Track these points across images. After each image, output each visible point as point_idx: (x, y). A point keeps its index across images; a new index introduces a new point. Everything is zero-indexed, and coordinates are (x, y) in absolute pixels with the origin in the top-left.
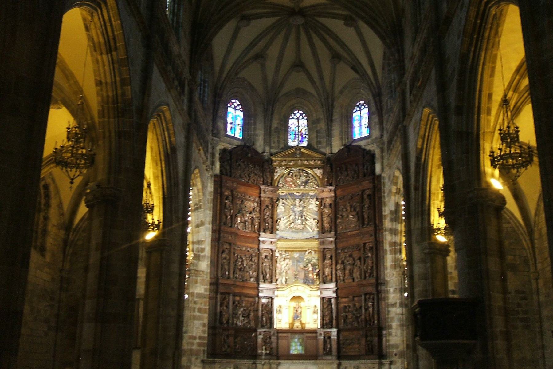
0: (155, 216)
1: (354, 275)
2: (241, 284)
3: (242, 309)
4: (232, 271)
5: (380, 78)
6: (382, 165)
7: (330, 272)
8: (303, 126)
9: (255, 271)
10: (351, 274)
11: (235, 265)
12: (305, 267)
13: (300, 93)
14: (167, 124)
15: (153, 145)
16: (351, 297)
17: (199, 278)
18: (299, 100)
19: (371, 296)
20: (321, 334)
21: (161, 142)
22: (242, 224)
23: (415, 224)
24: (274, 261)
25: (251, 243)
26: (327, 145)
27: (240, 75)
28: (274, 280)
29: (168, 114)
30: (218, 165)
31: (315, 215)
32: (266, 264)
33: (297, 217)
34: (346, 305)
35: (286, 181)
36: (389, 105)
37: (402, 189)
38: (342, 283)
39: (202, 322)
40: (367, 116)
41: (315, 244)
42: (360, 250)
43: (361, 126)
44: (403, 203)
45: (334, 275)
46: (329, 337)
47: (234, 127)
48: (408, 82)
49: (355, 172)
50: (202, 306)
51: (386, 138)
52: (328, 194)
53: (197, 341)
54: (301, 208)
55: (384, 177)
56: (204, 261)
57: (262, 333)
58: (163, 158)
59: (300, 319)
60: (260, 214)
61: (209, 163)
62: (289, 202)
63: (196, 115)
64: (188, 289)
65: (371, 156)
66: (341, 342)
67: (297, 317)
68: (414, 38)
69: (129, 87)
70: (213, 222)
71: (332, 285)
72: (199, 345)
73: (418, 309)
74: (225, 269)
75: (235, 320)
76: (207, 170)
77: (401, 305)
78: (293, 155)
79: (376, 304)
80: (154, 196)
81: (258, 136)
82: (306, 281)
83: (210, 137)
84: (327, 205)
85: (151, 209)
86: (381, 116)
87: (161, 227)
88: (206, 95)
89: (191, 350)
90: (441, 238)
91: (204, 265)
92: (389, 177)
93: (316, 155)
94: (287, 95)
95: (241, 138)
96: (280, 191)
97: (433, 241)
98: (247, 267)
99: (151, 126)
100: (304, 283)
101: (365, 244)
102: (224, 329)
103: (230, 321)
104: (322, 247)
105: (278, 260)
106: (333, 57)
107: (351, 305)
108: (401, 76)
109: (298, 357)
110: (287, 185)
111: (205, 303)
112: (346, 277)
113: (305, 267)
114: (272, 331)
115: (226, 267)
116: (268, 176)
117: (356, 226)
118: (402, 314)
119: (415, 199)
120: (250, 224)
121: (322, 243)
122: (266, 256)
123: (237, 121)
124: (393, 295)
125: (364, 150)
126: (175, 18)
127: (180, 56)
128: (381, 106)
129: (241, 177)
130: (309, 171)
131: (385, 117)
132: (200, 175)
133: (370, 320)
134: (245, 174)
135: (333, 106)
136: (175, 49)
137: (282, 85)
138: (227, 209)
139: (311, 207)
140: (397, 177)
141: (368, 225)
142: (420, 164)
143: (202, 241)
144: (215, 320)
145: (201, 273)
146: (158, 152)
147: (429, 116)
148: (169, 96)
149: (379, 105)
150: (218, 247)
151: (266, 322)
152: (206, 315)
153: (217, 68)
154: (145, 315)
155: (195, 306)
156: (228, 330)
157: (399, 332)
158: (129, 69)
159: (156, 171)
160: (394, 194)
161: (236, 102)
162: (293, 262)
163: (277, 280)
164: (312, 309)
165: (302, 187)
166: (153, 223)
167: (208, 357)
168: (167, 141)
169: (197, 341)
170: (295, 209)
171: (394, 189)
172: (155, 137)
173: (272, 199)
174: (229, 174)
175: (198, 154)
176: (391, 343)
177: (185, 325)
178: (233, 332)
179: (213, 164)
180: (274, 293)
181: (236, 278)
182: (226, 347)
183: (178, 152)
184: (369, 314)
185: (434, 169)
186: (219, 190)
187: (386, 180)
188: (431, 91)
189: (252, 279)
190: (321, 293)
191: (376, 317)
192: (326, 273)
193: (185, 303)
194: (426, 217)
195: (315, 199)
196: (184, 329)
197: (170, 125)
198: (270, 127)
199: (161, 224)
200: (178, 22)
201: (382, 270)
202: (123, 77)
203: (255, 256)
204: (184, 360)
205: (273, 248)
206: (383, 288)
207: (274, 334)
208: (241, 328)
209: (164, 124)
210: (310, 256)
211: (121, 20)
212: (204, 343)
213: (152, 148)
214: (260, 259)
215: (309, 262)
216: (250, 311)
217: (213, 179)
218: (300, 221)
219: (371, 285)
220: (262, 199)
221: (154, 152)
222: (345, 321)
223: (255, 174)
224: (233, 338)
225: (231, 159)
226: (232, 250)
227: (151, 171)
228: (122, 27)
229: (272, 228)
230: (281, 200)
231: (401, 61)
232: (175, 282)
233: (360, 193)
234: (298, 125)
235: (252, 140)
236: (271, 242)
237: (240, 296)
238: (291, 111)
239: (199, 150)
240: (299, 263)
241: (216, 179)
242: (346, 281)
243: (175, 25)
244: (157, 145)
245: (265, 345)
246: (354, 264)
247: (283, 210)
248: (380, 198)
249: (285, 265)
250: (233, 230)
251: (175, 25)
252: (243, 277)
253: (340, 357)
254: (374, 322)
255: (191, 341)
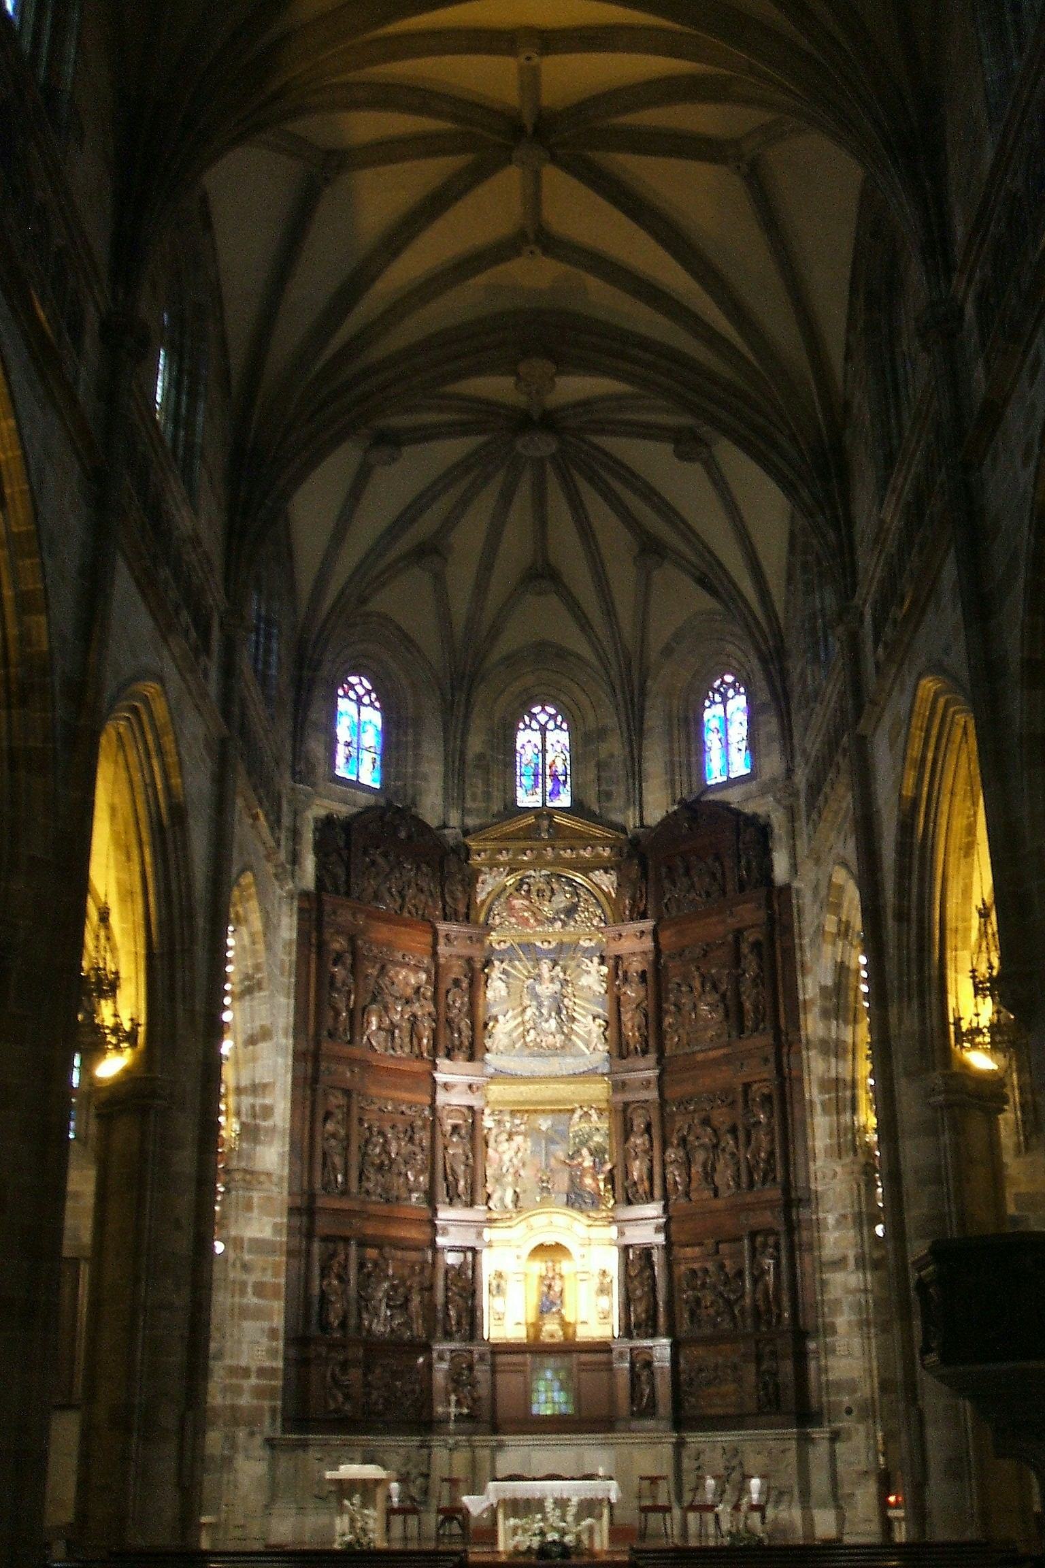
0: (126, 1007)
1: (717, 1178)
2: (384, 1209)
3: (386, 1285)
4: (354, 1174)
5: (779, 607)
6: (793, 854)
7: (645, 1171)
8: (558, 748)
9: (421, 1172)
10: (709, 1175)
11: (365, 1154)
12: (572, 1158)
13: (548, 654)
14: (157, 737)
15: (117, 801)
16: (710, 1242)
17: (256, 1196)
18: (544, 674)
19: (771, 1240)
20: (621, 1354)
21: (139, 790)
22: (383, 1034)
23: (900, 1020)
24: (479, 1141)
25: (408, 1089)
26: (628, 802)
27: (372, 606)
28: (480, 1198)
29: (160, 709)
30: (309, 863)
31: (597, 1004)
32: (456, 1149)
33: (545, 1011)
34: (696, 1266)
35: (512, 908)
36: (809, 681)
37: (857, 923)
38: (683, 1201)
39: (266, 1325)
40: (743, 718)
41: (599, 1090)
42: (734, 1102)
43: (726, 745)
44: (863, 960)
45: (657, 1181)
46: (648, 1364)
47: (354, 754)
48: (868, 611)
49: (713, 875)
50: (268, 1278)
51: (801, 778)
52: (635, 942)
53: (253, 1381)
54: (557, 987)
55: (798, 891)
56: (271, 1143)
57: (447, 1356)
58: (146, 836)
59: (559, 1312)
60: (436, 1005)
61: (283, 856)
62: (521, 968)
63: (243, 714)
64: (223, 1227)
65: (762, 832)
66: (683, 1377)
67: (549, 1304)
68: (883, 483)
69: (43, 619)
70: (299, 1029)
71: (653, 1210)
72: (259, 1393)
73: (931, 1268)
74: (334, 1168)
75: (365, 1316)
76: (276, 876)
77: (861, 1263)
78: (530, 833)
79: (784, 1261)
80: (117, 944)
81: (425, 778)
82: (576, 1199)
83: (285, 782)
84: (633, 975)
85: (109, 986)
86: (785, 717)
87: (141, 1039)
88: (273, 659)
89: (233, 1408)
90: (981, 1060)
91: (272, 1156)
92: (816, 889)
93: (598, 832)
94: (511, 660)
95: (378, 786)
96: (494, 936)
97: (956, 1068)
98: (400, 1159)
99: (107, 741)
100: (570, 1203)
101: (747, 1086)
102: (332, 1346)
103: (352, 1321)
104: (620, 1098)
105: (492, 1143)
106: (643, 551)
107: (710, 1266)
108: (848, 591)
109: (556, 1425)
110: (513, 920)
111: (276, 1267)
112: (694, 1185)
113: (572, 1158)
114: (477, 1349)
115: (338, 1160)
116: (459, 895)
117: (719, 1036)
118: (866, 1291)
119: (899, 948)
120: (406, 1034)
121: (619, 1087)
122: (455, 1128)
123: (363, 736)
124: (837, 1234)
125: (738, 813)
126: (182, 433)
127: (196, 541)
128: (784, 689)
129: (377, 897)
130: (579, 878)
131: (797, 721)
132: (258, 893)
133: (769, 1311)
134: (389, 889)
135: (643, 693)
136: (183, 520)
137: (495, 632)
138: (338, 991)
139: (585, 981)
140: (841, 888)
141: (756, 1029)
142: (912, 844)
143: (265, 1086)
144: (307, 1322)
145: (263, 1178)
146: (131, 820)
147: (935, 701)
148: (165, 653)
149: (778, 684)
150: (313, 1103)
151: (459, 1323)
152: (278, 1305)
153: (305, 580)
154: (96, 1304)
155: (245, 1277)
156: (344, 1347)
157: (856, 1342)
158: (43, 564)
159: (125, 876)
160: (829, 938)
161: (360, 684)
162: (536, 1143)
163: (489, 1197)
164: (595, 1283)
165: (558, 924)
166: (116, 1029)
167: (284, 1431)
168: (159, 786)
169: (253, 1381)
170: (539, 989)
171: (831, 926)
172: (123, 775)
173: (469, 960)
174: (342, 889)
175: (252, 831)
176: (832, 1377)
177: (215, 1334)
178: (361, 1353)
179: (295, 859)
180: (479, 1235)
181: (368, 1192)
182: (340, 1398)
183: (191, 822)
184: (766, 1286)
185: (952, 859)
186: (314, 935)
187: (807, 899)
188: (945, 622)
189: (415, 1195)
190: (621, 1233)
191: (785, 1299)
192: (636, 1175)
193: (217, 1268)
194: (934, 998)
195: (596, 960)
196: (213, 1346)
197: (168, 743)
198: (462, 754)
199: (142, 1030)
200: (190, 447)
201: (800, 1160)
202: (24, 588)
203: (424, 1128)
204: (214, 1439)
205: (477, 1103)
206: (804, 1213)
207: (482, 1358)
208: (382, 1351)
209: (150, 737)
210: (585, 1126)
211: (17, 418)
212: (274, 1388)
213: (113, 810)
214: (439, 1135)
215: (584, 1143)
216: (410, 1288)
217: (296, 903)
218: (553, 1024)
219: (770, 1204)
220: (442, 961)
221: (120, 820)
222: (692, 1314)
223: (422, 891)
224: (360, 1372)
225: (348, 845)
226: (355, 1112)
227: (109, 873)
228: (21, 438)
229: (472, 1045)
230: (497, 963)
231: (846, 548)
232: (184, 1203)
233: (730, 937)
234: (543, 745)
235: (410, 792)
236: (470, 1086)
237: (380, 1247)
238: (522, 707)
239: (255, 817)
240: (552, 1147)
241: (306, 905)
242: (694, 1196)
243: (180, 452)
244: (127, 797)
245: (455, 1391)
246: (715, 1146)
247: (504, 993)
248: (790, 952)
249: (512, 1153)
250: (355, 1051)
251: (180, 452)
252: (386, 1189)
253: (681, 1422)
254: (779, 1316)
255: (234, 1381)
